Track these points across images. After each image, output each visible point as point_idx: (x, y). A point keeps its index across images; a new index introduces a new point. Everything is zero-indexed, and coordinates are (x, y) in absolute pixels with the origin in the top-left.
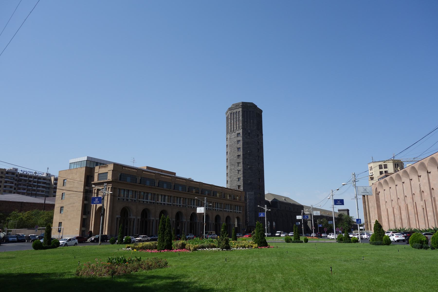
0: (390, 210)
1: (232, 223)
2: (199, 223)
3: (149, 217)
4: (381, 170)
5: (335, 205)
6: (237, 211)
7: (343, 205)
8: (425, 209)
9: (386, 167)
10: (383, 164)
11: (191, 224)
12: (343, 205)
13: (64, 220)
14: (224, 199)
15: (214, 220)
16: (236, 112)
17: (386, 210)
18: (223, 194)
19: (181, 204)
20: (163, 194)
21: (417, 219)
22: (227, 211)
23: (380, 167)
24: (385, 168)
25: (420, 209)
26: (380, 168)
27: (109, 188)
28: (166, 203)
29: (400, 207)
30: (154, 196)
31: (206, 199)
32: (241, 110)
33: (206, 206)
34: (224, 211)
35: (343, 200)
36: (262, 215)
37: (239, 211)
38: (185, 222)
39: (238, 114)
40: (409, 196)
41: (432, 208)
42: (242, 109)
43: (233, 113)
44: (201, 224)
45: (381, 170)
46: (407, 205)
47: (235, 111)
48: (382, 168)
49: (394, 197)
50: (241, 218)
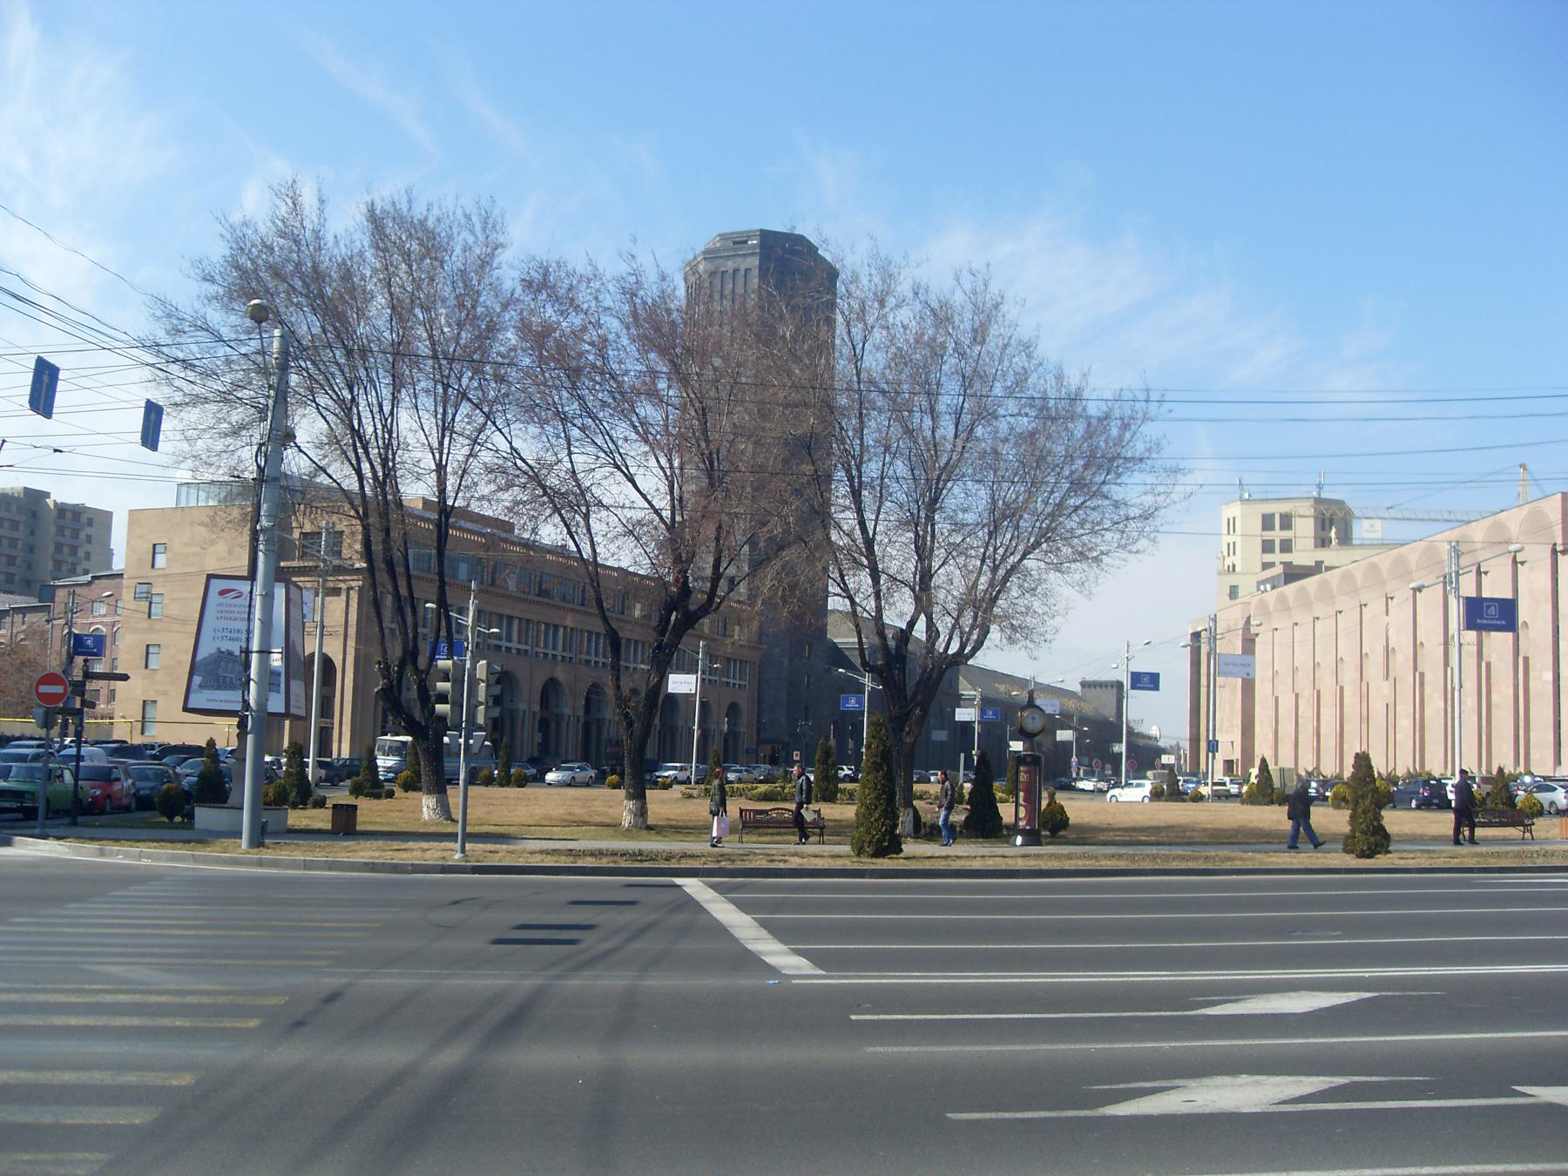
0: (1286, 703)
1: (680, 723)
2: (524, 712)
3: (557, 706)
4: (1269, 535)
5: (1132, 688)
6: (732, 681)
7: (1158, 690)
8: (1391, 709)
9: (1287, 521)
10: (1277, 509)
11: (587, 726)
12: (1158, 690)
13: (165, 693)
14: (621, 617)
15: (537, 696)
16: (736, 271)
17: (1271, 702)
18: (581, 588)
19: (559, 652)
20: (507, 612)
21: (1364, 738)
22: (590, 661)
23: (1267, 522)
24: (1282, 528)
25: (1378, 708)
26: (1265, 528)
27: (349, 589)
28: (514, 645)
29: (1319, 692)
30: (527, 627)
31: (704, 646)
32: (757, 263)
33: (703, 672)
34: (488, 649)
35: (1158, 674)
36: (852, 703)
37: (738, 682)
38: (524, 712)
39: (743, 279)
40: (1351, 661)
41: (1550, 606)
42: (760, 261)
43: (723, 272)
44: (534, 718)
45: (1269, 535)
46: (1342, 689)
47: (730, 265)
48: (1272, 528)
49: (1303, 660)
50: (744, 706)
